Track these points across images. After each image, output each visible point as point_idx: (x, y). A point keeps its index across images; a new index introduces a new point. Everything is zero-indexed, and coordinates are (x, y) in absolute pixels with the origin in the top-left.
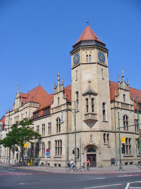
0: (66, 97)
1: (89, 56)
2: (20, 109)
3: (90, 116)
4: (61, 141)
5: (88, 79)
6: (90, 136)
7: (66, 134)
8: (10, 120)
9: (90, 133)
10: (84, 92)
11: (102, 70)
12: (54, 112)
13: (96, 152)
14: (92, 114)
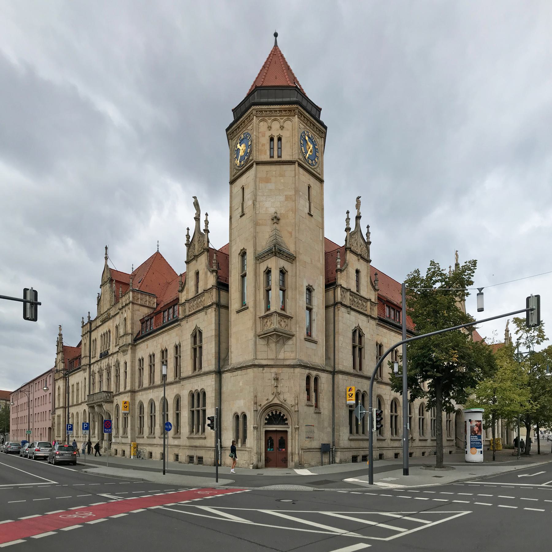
0: (215, 268)
1: (276, 140)
2: (112, 313)
3: (275, 319)
4: (204, 394)
5: (272, 211)
6: (274, 379)
7: (539, 451)
8: (92, 342)
9: (274, 370)
10: (260, 250)
11: (309, 188)
12: (187, 313)
13: (287, 424)
14: (280, 315)
